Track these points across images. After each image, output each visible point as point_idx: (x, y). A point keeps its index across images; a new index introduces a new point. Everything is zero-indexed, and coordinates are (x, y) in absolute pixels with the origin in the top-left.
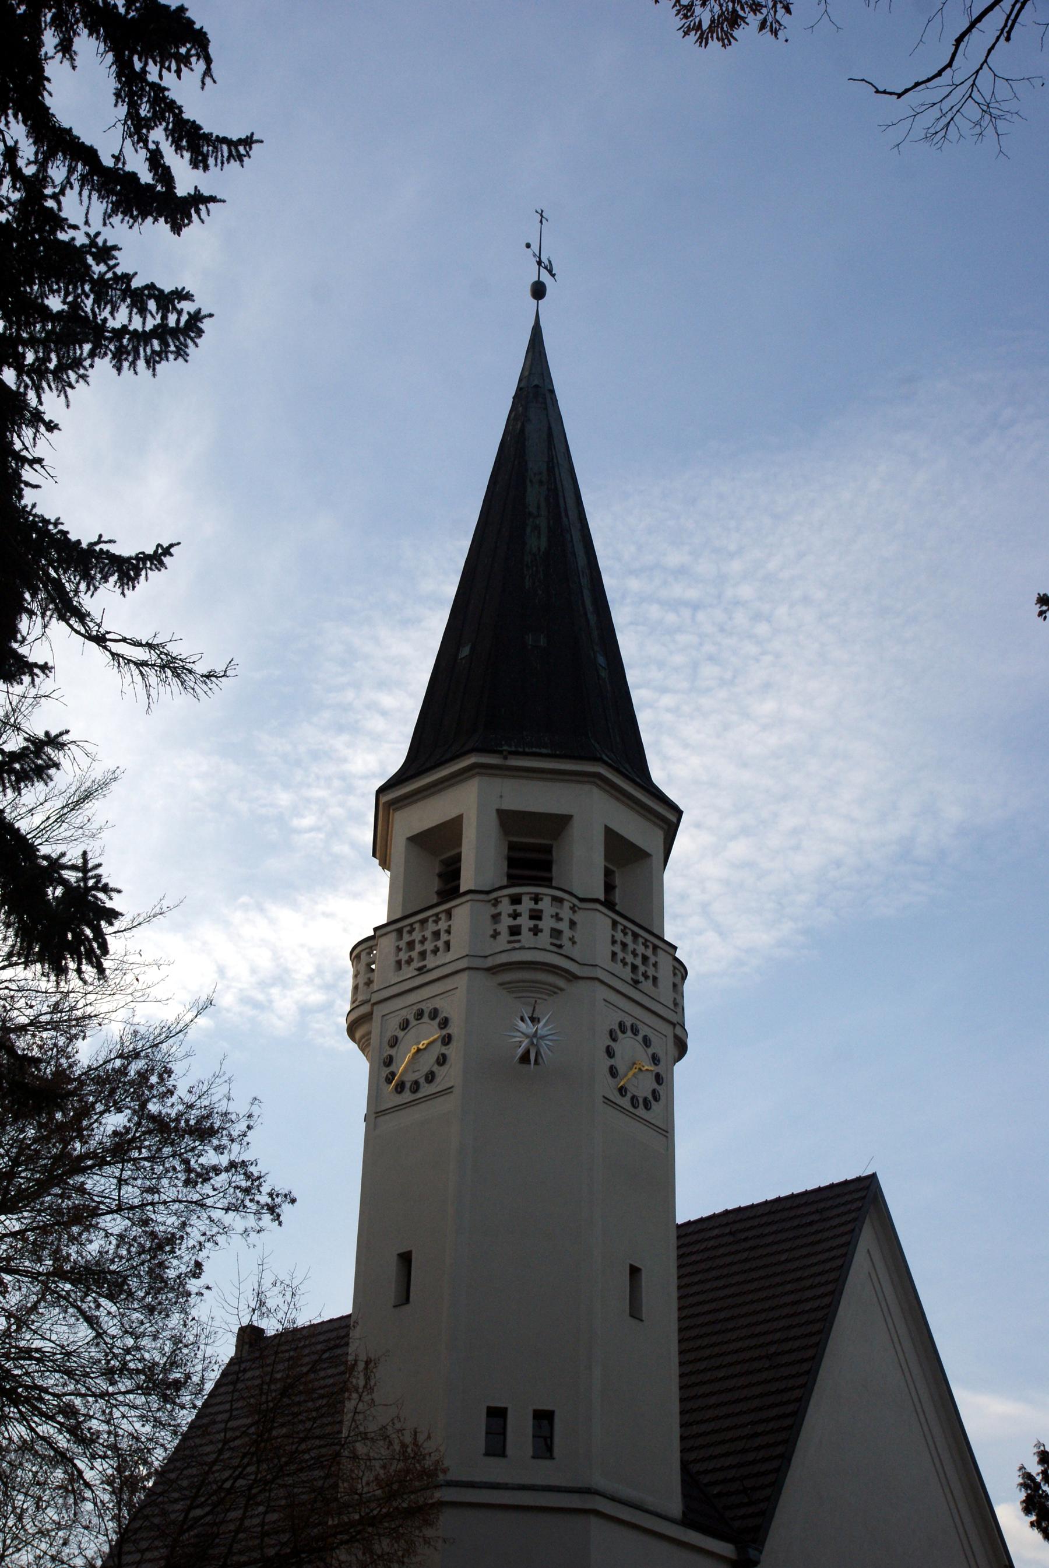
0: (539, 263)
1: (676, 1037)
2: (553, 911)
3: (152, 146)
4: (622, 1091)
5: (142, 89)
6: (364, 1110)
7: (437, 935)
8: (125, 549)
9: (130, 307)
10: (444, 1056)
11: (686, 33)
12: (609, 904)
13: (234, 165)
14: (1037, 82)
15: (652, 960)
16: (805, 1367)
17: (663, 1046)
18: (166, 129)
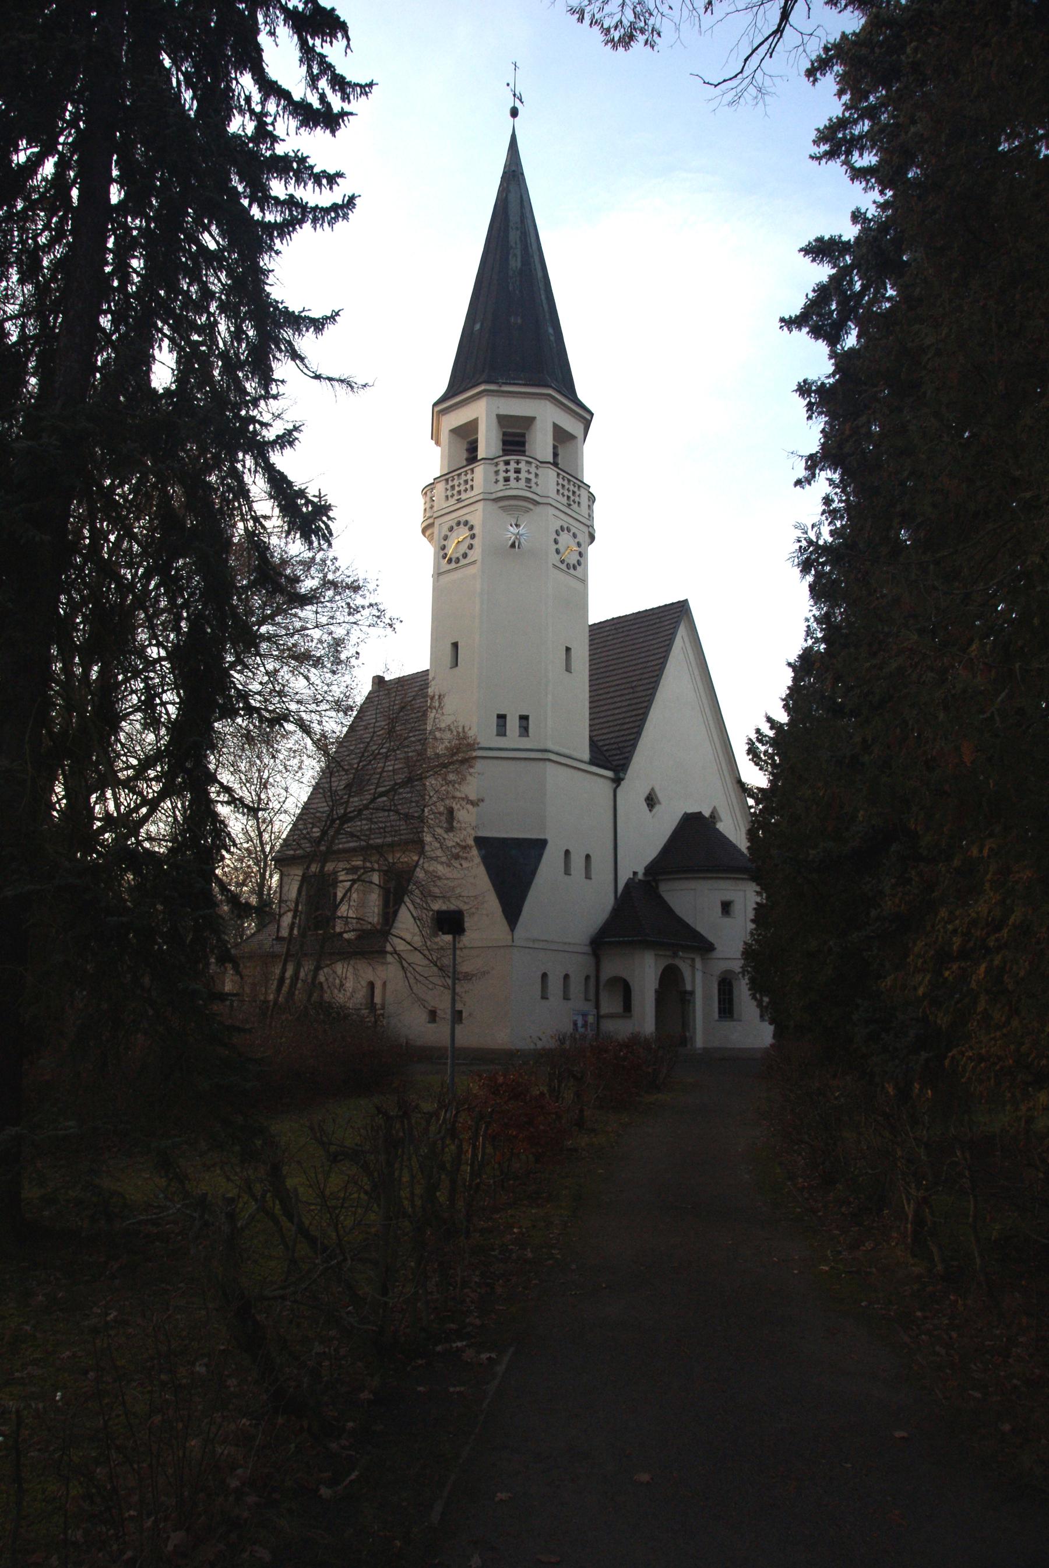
0: (515, 95)
1: (589, 532)
2: (526, 469)
3: (321, 91)
4: (562, 562)
5: (314, 56)
6: (432, 573)
7: (466, 482)
8: (316, 314)
9: (314, 183)
10: (472, 545)
11: (606, 44)
12: (555, 464)
13: (364, 97)
14: (785, 78)
15: (578, 493)
16: (649, 692)
17: (583, 537)
18: (327, 80)
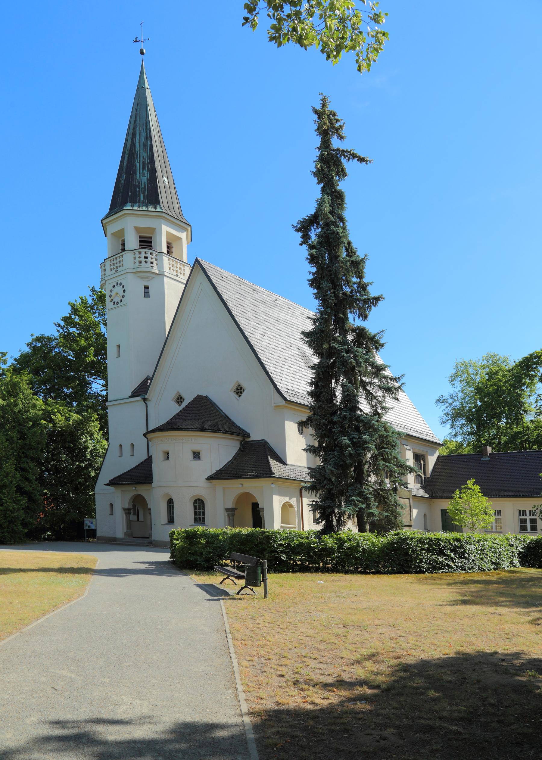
15: (183, 268)
